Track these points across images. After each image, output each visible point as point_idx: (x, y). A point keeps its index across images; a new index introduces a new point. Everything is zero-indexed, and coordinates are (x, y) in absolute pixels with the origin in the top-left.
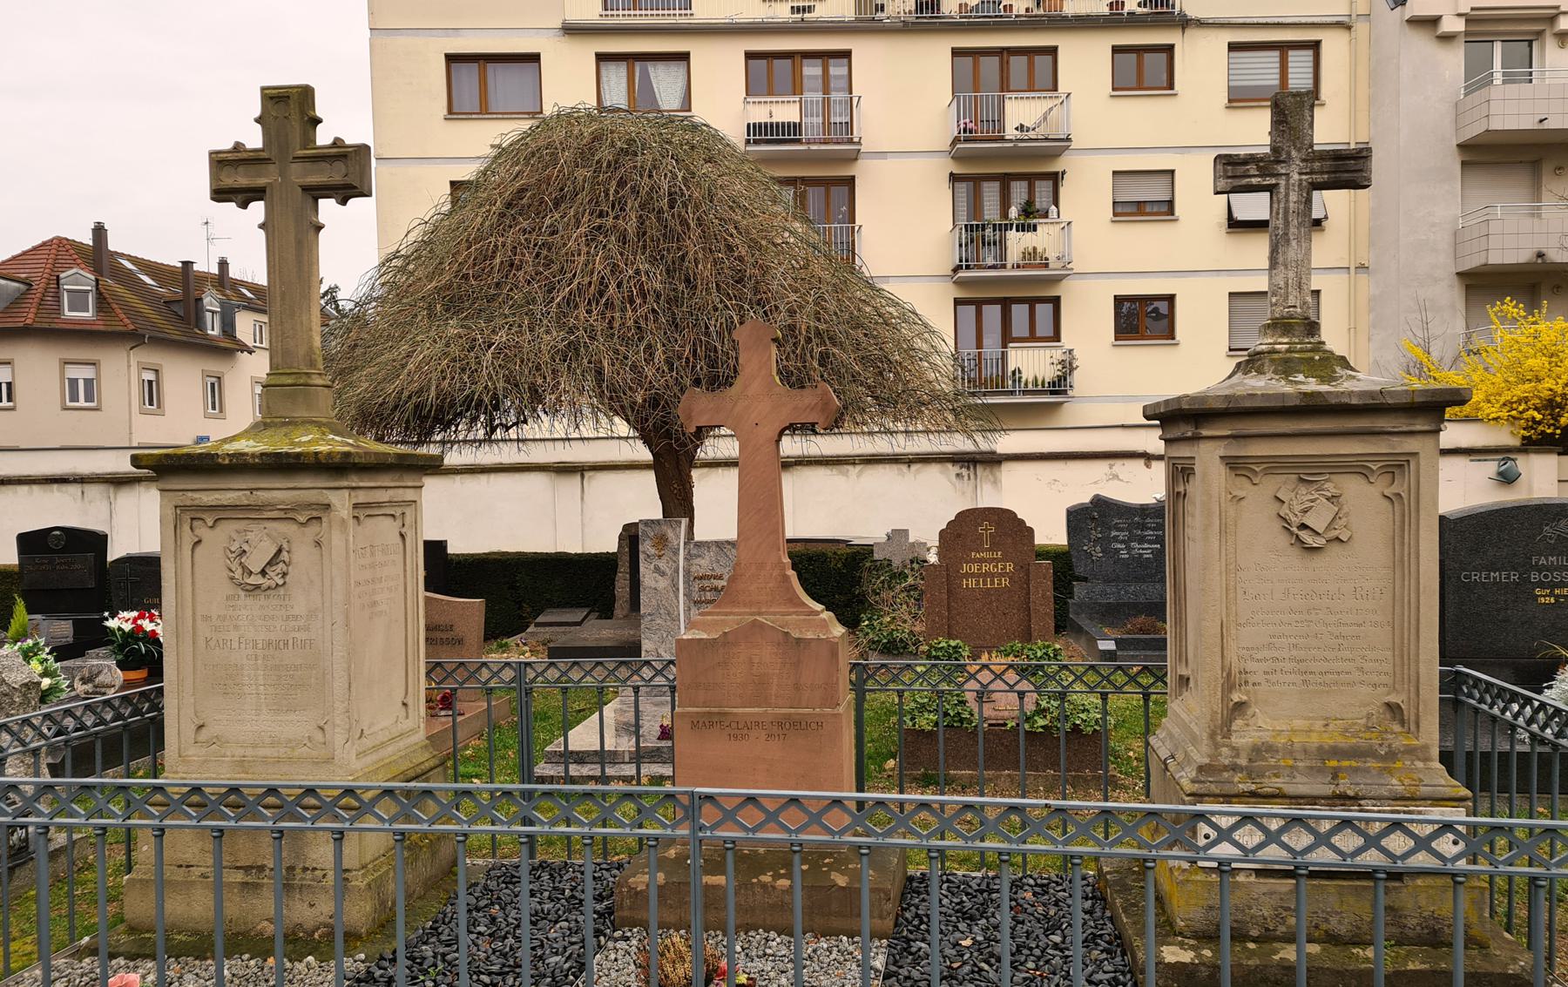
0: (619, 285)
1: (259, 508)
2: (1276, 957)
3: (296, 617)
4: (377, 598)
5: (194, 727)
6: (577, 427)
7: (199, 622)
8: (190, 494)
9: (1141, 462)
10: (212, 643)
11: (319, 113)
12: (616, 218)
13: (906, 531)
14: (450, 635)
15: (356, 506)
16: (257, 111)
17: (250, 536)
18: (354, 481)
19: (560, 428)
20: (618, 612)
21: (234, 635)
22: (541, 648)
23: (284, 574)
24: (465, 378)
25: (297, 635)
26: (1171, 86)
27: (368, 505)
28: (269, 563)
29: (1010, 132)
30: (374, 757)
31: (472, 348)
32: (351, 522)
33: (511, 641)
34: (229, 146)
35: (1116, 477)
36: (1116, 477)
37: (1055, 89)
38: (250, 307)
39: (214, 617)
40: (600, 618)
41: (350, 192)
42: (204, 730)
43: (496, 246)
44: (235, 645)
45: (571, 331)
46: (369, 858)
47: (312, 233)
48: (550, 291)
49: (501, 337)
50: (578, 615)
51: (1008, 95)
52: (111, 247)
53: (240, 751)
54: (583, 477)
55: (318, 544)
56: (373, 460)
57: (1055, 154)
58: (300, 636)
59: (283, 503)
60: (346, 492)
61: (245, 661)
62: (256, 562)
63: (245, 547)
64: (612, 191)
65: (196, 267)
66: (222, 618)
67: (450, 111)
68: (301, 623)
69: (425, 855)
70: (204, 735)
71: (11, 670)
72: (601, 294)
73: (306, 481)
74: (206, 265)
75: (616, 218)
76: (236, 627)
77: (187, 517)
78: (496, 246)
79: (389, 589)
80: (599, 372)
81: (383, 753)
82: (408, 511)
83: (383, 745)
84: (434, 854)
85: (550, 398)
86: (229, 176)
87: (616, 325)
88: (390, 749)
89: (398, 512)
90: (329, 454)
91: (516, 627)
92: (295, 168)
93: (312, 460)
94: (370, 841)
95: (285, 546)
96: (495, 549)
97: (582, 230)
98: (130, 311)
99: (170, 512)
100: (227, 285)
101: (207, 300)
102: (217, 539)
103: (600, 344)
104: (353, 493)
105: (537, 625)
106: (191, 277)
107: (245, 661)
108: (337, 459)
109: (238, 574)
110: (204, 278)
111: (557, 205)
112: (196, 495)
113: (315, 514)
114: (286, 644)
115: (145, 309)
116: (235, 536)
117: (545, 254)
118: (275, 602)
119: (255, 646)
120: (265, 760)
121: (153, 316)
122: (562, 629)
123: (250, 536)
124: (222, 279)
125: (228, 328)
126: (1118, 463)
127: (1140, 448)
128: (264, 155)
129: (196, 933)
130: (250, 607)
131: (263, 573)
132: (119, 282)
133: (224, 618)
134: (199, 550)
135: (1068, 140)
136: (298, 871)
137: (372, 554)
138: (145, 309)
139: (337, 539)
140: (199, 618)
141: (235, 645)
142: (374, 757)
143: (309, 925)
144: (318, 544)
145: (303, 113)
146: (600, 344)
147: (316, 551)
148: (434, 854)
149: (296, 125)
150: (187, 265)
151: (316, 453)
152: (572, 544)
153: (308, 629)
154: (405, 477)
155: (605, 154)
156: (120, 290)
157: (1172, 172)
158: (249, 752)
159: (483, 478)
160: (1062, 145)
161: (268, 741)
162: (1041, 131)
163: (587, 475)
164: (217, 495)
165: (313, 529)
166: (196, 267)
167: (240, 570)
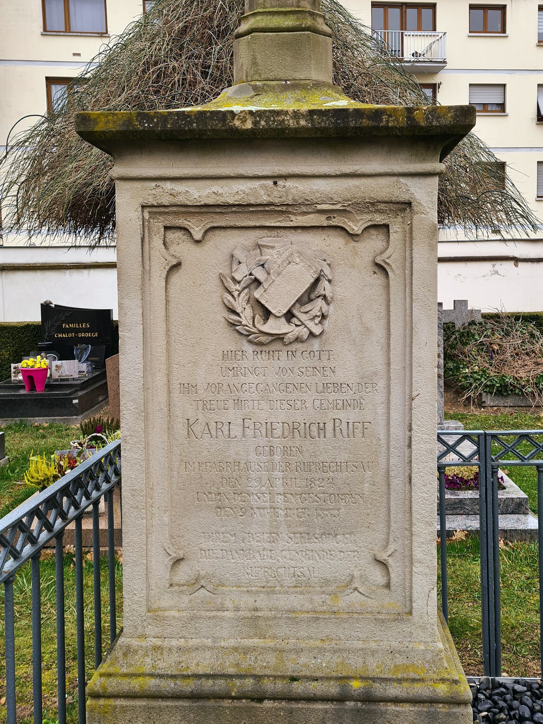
2: (464, 539)
3: (338, 387)
5: (168, 562)
7: (176, 394)
8: (168, 185)
9: (512, 263)
10: (198, 428)
13: (466, 302)
17: (268, 255)
21: (233, 415)
26: (504, 31)
28: (300, 301)
29: (408, 56)
35: (497, 272)
36: (497, 272)
37: (434, 29)
42: (183, 567)
44: (236, 431)
51: (406, 33)
57: (434, 72)
58: (349, 415)
59: (331, 200)
61: (253, 457)
62: (279, 296)
63: (260, 274)
68: (349, 396)
70: (184, 573)
76: (238, 402)
77: (158, 224)
93: (402, 121)
107: (253, 457)
109: (247, 315)
112: (179, 187)
113: (379, 219)
114: (322, 429)
118: (302, 362)
120: (292, 616)
126: (498, 264)
127: (510, 254)
130: (262, 369)
131: (289, 316)
133: (218, 387)
134: (175, 278)
135: (445, 62)
140: (176, 386)
141: (236, 431)
144: (381, 268)
147: (379, 279)
154: (259, 218)
157: (504, 85)
158: (262, 601)
159: (85, 272)
160: (439, 66)
161: (289, 581)
162: (428, 56)
164: (216, 187)
165: (373, 244)
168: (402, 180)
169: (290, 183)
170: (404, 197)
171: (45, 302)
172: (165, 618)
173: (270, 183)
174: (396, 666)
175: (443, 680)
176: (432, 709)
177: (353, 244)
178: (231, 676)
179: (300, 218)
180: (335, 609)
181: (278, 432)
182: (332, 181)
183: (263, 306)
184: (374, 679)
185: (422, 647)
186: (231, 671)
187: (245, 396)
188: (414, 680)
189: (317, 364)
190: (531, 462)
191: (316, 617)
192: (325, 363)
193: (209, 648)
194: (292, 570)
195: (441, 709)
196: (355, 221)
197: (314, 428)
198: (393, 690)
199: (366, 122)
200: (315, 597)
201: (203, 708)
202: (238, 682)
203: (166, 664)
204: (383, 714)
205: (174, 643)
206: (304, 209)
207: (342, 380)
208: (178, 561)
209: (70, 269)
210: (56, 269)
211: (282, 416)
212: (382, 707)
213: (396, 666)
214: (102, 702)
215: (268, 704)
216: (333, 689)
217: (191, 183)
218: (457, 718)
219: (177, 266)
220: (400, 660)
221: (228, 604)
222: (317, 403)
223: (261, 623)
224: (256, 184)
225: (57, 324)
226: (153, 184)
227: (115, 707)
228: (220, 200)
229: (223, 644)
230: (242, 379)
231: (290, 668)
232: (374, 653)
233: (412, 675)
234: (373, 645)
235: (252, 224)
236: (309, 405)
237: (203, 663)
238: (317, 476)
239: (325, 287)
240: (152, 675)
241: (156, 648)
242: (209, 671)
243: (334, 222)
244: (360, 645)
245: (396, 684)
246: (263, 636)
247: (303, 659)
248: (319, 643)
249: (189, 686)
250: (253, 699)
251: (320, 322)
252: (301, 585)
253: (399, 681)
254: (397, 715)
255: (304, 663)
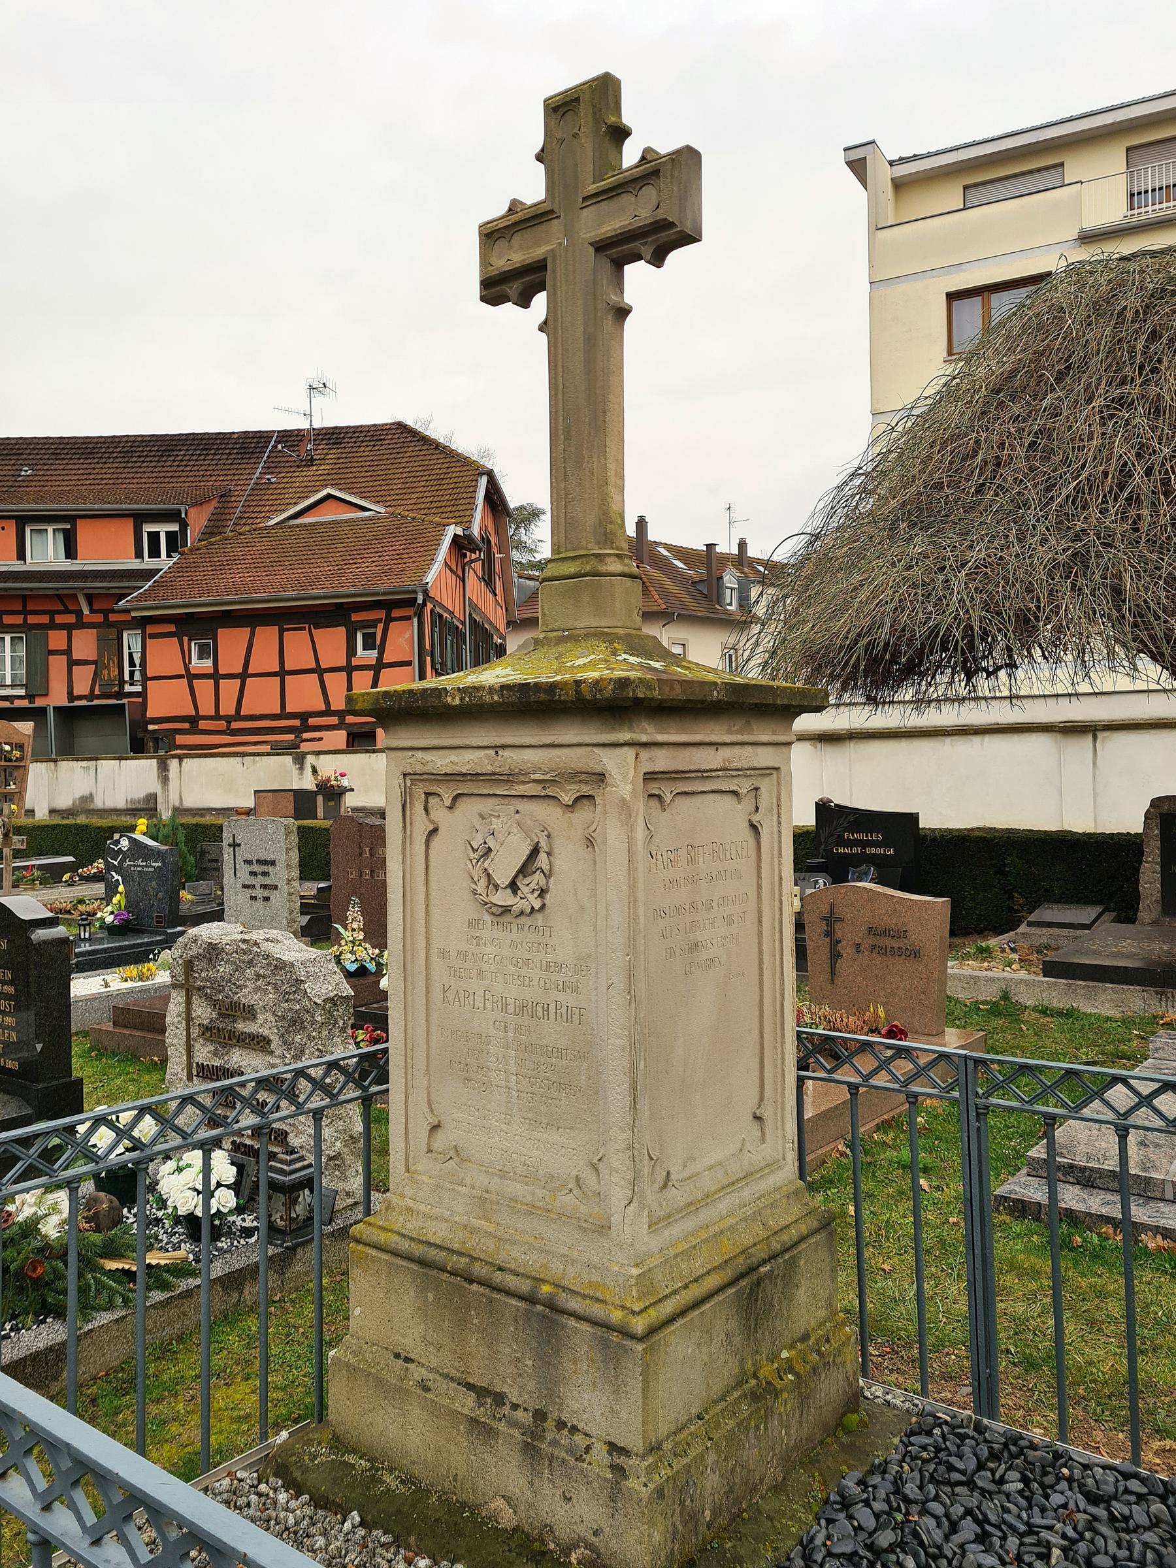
0: (1149, 472)
1: (508, 778)
3: (559, 967)
4: (700, 936)
6: (1087, 675)
7: (434, 958)
8: (420, 754)
10: (451, 995)
11: (627, 119)
12: (1146, 382)
14: (902, 943)
15: (651, 777)
16: (536, 138)
17: (496, 824)
18: (646, 731)
19: (1064, 677)
20: (1144, 915)
22: (1034, 957)
23: (543, 893)
24: (930, 608)
25: (561, 997)
27: (679, 775)
30: (690, 1224)
31: (942, 569)
32: (640, 805)
33: (993, 942)
34: (503, 209)
38: (763, 581)
39: (453, 954)
40: (1118, 920)
41: (665, 236)
42: (440, 1135)
43: (977, 442)
44: (479, 1002)
45: (1077, 538)
46: (664, 1429)
47: (609, 322)
48: (1048, 489)
49: (979, 553)
50: (1086, 914)
52: (651, 537)
53: (483, 1180)
54: (1095, 738)
55: (590, 842)
56: (677, 693)
60: (630, 753)
62: (504, 868)
63: (491, 843)
64: (1139, 347)
65: (718, 549)
66: (463, 955)
67: (950, 353)
68: (567, 977)
69: (786, 1404)
70: (441, 1141)
71: (316, 978)
72: (1121, 487)
73: (570, 732)
74: (727, 546)
75: (1146, 382)
76: (480, 973)
78: (977, 442)
79: (728, 921)
80: (1118, 591)
81: (705, 1215)
82: (765, 785)
83: (708, 1198)
84: (804, 1399)
85: (1046, 631)
86: (500, 257)
87: (1144, 525)
88: (723, 1206)
89: (744, 786)
90: (597, 682)
91: (1004, 923)
92: (588, 215)
94: (692, 1369)
95: (543, 844)
96: (980, 825)
97: (1097, 403)
98: (664, 593)
99: (397, 781)
100: (745, 563)
101: (726, 578)
102: (459, 823)
103: (1119, 553)
104: (644, 754)
105: (1030, 924)
106: (714, 559)
108: (608, 693)
110: (725, 559)
111: (1060, 379)
112: (427, 756)
113: (585, 790)
114: (546, 1010)
115: (675, 589)
116: (478, 823)
117: (1041, 446)
118: (531, 937)
119: (504, 1008)
121: (686, 599)
122: (1065, 932)
123: (496, 824)
124: (741, 559)
125: (745, 605)
128: (546, 207)
129: (408, 1480)
130: (499, 942)
131: (513, 886)
132: (657, 567)
134: (435, 843)
136: (550, 1424)
137: (692, 860)
138: (675, 589)
139: (614, 837)
140: (434, 951)
141: (479, 1002)
142: (690, 1224)
143: (563, 1532)
145: (598, 119)
146: (1119, 553)
148: (804, 1399)
149: (587, 145)
150: (710, 547)
151: (578, 683)
152: (1080, 821)
153: (575, 989)
155: (1131, 301)
156: (656, 574)
159: (976, 740)
161: (521, 1170)
163: (1100, 735)
165: (583, 815)
166: (718, 549)
167: (483, 881)
168: (596, 750)
169: (506, 753)
170: (598, 769)
171: (821, 800)
172: (417, 1181)
173: (492, 752)
174: (590, 1282)
175: (623, 1307)
176: (606, 1335)
177: (569, 814)
178: (454, 1252)
179: (522, 787)
180: (550, 1207)
181: (511, 1008)
182: (539, 751)
183: (489, 875)
184: (564, 1289)
185: (616, 1268)
186: (456, 1246)
187: (486, 967)
188: (598, 1300)
189: (540, 940)
190: (1036, 1107)
191: (531, 1210)
192: (547, 940)
193: (447, 1221)
194: (523, 1159)
195: (614, 1337)
196: (566, 792)
197: (540, 1008)
198: (574, 1304)
199: (543, 697)
200: (537, 1191)
201: (425, 1275)
202: (455, 1258)
203: (412, 1227)
204: (564, 1326)
205: (422, 1208)
206: (522, 778)
207: (560, 960)
208: (436, 1127)
209: (952, 735)
210: (930, 736)
211: (513, 993)
212: (564, 1319)
213: (590, 1282)
214: (360, 1247)
215: (475, 1287)
216: (524, 1287)
217: (435, 752)
218: (626, 1352)
219: (435, 830)
220: (595, 1277)
221: (468, 1181)
222: (542, 981)
223: (488, 1206)
224: (483, 753)
225: (837, 832)
226: (410, 753)
227: (367, 1255)
228: (456, 769)
229: (457, 1219)
230: (484, 949)
231: (502, 1258)
232: (574, 1262)
233: (599, 1295)
234: (575, 1254)
235: (486, 792)
236: (535, 982)
237: (438, 1232)
238: (543, 1060)
239: (542, 860)
240: (398, 1233)
241: (409, 1209)
242: (439, 1242)
243: (549, 792)
244: (563, 1250)
245: (580, 1299)
246: (489, 1220)
247: (515, 1253)
248: (531, 1240)
249: (418, 1250)
250: (465, 1280)
251: (539, 895)
252: (529, 1178)
253: (585, 1297)
254: (576, 1331)
255: (515, 1256)
